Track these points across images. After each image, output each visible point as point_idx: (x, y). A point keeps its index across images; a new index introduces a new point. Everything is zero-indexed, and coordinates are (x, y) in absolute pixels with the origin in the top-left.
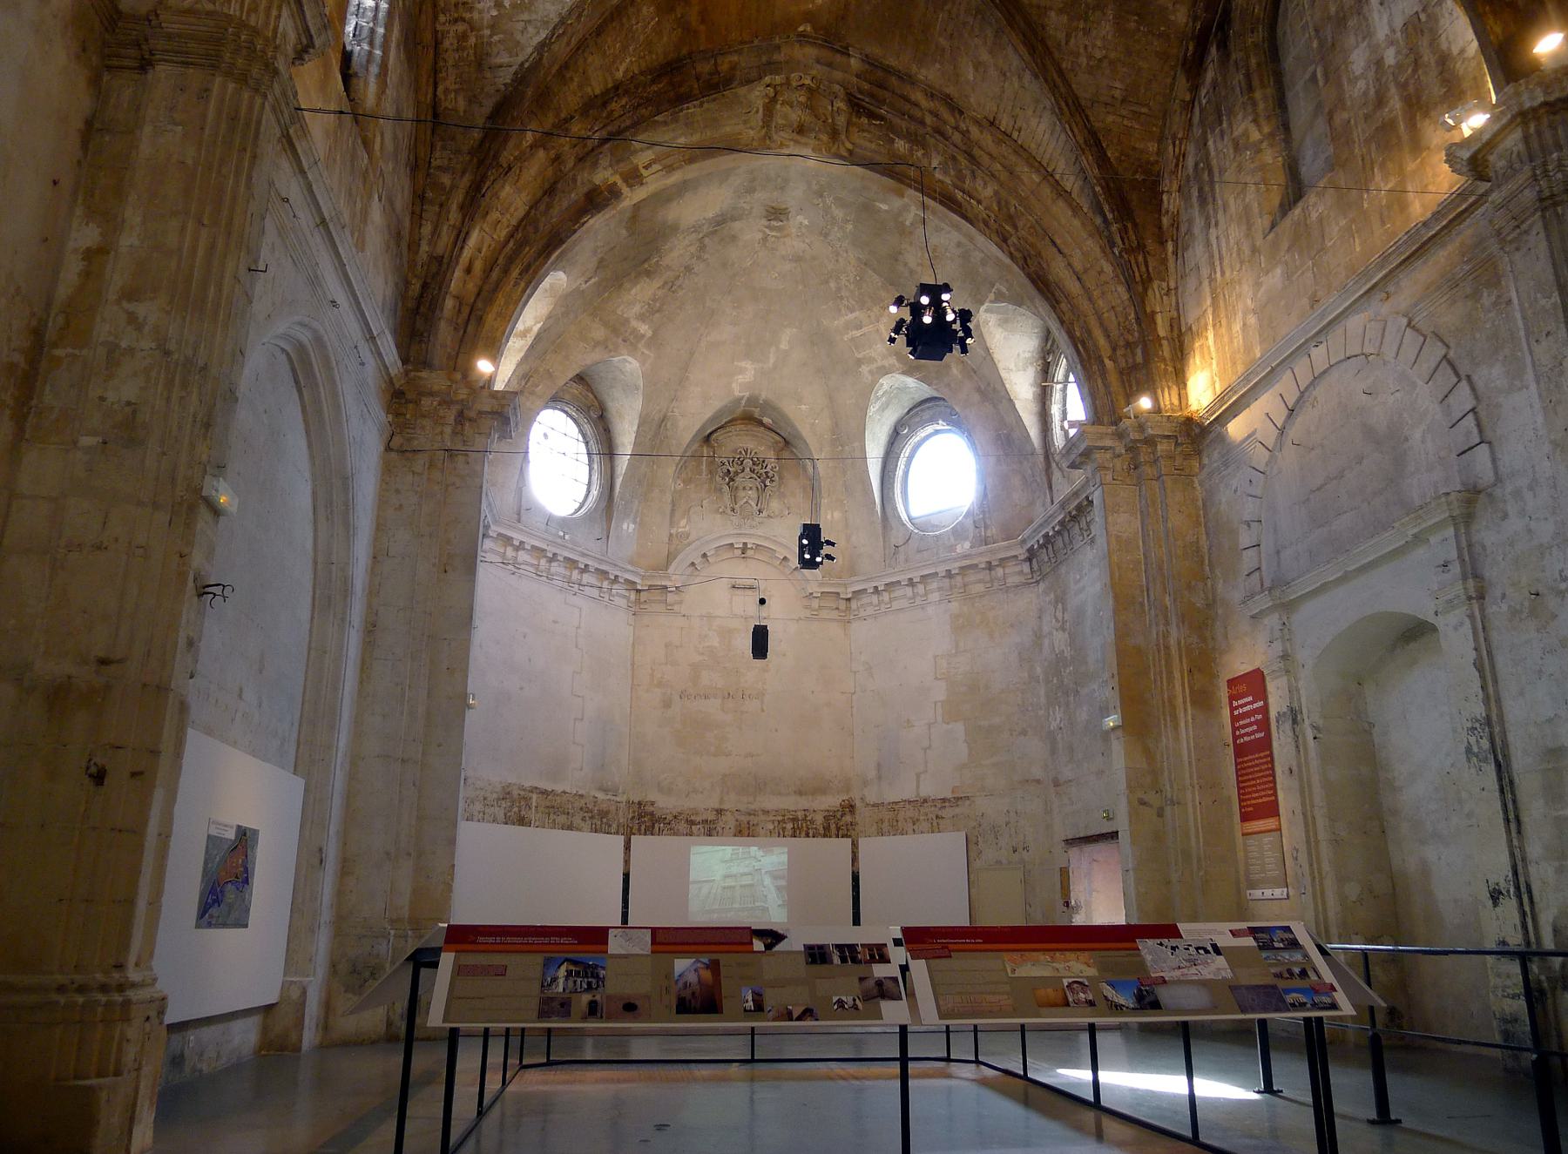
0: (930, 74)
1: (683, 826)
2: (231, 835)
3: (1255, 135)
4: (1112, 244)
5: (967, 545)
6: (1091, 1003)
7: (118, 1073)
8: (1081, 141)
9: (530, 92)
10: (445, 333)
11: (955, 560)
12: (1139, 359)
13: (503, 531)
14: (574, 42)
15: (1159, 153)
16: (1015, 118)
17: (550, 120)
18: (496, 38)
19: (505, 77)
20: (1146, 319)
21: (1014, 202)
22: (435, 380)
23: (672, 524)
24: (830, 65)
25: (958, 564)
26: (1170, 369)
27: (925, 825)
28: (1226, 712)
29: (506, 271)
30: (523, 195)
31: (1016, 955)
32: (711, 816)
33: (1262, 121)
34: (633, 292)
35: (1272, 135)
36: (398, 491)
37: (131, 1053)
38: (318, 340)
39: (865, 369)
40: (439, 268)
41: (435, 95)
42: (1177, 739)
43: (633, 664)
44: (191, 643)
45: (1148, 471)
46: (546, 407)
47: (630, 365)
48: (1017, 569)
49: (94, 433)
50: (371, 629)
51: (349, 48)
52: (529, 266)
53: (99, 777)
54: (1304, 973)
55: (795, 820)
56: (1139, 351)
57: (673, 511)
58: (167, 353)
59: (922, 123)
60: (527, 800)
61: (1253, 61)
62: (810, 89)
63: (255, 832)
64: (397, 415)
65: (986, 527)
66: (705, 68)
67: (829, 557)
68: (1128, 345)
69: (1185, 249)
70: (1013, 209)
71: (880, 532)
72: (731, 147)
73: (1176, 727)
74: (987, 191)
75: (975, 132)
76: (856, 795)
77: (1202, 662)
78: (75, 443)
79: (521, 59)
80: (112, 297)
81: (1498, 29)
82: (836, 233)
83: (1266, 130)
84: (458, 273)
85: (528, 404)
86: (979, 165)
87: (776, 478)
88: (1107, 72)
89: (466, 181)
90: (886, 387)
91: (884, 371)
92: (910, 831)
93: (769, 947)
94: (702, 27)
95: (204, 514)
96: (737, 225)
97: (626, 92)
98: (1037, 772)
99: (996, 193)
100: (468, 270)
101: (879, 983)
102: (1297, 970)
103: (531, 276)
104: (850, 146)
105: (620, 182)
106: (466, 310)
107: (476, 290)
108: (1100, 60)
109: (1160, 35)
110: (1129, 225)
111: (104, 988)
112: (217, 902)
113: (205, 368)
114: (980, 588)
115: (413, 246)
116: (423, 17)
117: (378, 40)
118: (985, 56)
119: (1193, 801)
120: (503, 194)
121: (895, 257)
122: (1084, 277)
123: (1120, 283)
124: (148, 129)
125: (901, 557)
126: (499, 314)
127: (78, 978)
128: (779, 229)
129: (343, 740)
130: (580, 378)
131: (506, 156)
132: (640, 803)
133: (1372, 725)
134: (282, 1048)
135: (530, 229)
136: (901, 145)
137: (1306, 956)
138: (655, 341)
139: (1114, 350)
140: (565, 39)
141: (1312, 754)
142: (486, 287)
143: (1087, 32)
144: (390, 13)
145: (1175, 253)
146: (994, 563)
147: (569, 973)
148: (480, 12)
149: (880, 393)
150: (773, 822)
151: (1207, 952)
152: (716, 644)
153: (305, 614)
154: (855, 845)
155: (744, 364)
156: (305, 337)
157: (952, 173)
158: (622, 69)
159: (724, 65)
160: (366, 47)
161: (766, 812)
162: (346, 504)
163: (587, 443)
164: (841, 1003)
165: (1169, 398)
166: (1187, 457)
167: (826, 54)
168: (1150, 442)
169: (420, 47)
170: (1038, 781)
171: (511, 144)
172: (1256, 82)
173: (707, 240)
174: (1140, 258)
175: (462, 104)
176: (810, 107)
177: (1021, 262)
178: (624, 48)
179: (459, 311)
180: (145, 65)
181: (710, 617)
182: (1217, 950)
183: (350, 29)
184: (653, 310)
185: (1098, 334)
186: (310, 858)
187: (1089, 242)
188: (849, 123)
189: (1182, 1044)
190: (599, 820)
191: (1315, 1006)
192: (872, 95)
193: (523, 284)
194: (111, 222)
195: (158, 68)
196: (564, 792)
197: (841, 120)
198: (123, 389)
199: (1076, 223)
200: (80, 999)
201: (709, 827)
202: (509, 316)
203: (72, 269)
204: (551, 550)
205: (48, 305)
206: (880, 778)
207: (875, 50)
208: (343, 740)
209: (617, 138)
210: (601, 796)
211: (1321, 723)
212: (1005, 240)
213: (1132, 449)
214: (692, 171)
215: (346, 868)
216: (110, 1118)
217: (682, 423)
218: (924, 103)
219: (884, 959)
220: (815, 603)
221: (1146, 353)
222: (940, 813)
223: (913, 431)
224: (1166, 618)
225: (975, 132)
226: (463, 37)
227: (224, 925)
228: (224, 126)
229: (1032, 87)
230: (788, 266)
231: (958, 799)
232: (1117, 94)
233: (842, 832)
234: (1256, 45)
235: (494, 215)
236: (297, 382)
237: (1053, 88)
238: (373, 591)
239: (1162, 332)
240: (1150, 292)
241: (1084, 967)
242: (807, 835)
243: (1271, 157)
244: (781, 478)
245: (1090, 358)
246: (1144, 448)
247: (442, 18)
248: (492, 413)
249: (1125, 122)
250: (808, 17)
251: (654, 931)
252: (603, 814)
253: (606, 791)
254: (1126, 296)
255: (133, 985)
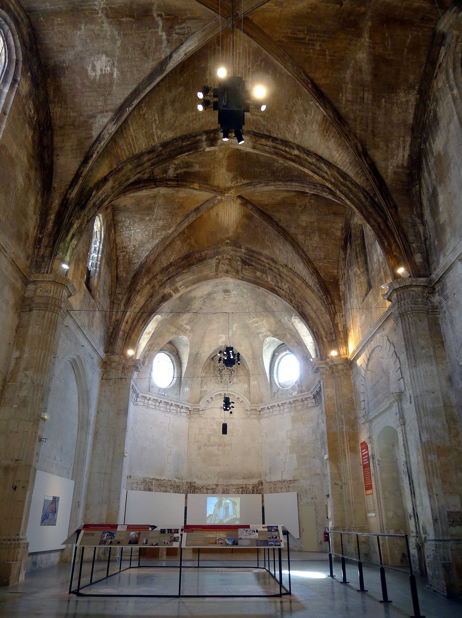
0: (266, 252)
1: (205, 490)
2: (51, 499)
3: (359, 272)
4: (324, 302)
5: (296, 393)
6: (222, 543)
7: (16, 561)
8: (312, 272)
9: (144, 270)
10: (120, 342)
11: (291, 398)
12: (334, 338)
13: (143, 395)
14: (156, 255)
15: (337, 273)
16: (292, 264)
17: (151, 276)
18: (134, 255)
19: (137, 266)
20: (335, 325)
21: (294, 289)
22: (116, 358)
23: (201, 387)
24: (236, 251)
25: (292, 400)
26: (343, 341)
27: (284, 490)
28: (361, 454)
29: (138, 322)
30: (143, 299)
31: (208, 532)
32: (214, 487)
33: (361, 268)
34: (184, 317)
35: (363, 272)
36: (105, 391)
37: (19, 556)
38: (78, 356)
39: (260, 336)
40: (118, 323)
41: (117, 272)
42: (346, 463)
43: (188, 435)
44: (37, 454)
45: (336, 374)
46: (159, 352)
47: (185, 338)
48: (311, 401)
49: (16, 404)
50: (96, 433)
51: (90, 269)
52: (145, 320)
53: (15, 488)
54: (276, 537)
55: (242, 488)
56: (334, 335)
57: (202, 383)
58: (34, 383)
59: (265, 267)
60: (151, 483)
61: (358, 249)
62: (230, 259)
63: (58, 498)
64: (105, 368)
65: (302, 387)
66: (197, 255)
67: (233, 407)
68: (331, 334)
69: (346, 303)
70: (294, 292)
71: (269, 388)
72: (206, 278)
73: (346, 459)
74: (286, 286)
75: (281, 268)
76: (263, 479)
77: (354, 437)
78: (12, 406)
79: (141, 261)
80: (21, 370)
81: (392, 263)
82: (245, 296)
83: (362, 270)
84: (124, 324)
85: (152, 353)
86: (283, 278)
87: (235, 371)
88: (318, 250)
89: (126, 297)
90: (268, 341)
91: (267, 336)
92: (280, 491)
93: (152, 529)
94: (196, 245)
95: (41, 421)
96: (215, 295)
97: (174, 265)
98: (319, 471)
99: (289, 287)
100: (127, 323)
101: (175, 538)
102: (275, 537)
103: (146, 322)
104: (242, 276)
105: (172, 292)
106: (126, 335)
107: (129, 328)
108: (316, 247)
109: (333, 239)
110: (328, 296)
111: (14, 540)
112: (47, 518)
113: (42, 385)
114: (300, 408)
115: (110, 317)
116: (113, 253)
117: (98, 266)
118: (281, 247)
119: (351, 483)
120: (137, 299)
121: (265, 303)
122: (317, 312)
123: (327, 314)
124: (31, 327)
125: (276, 397)
126: (136, 335)
127: (9, 538)
128: (228, 295)
129: (86, 469)
130: (170, 343)
131: (138, 288)
132: (190, 483)
133: (397, 459)
134: (66, 562)
135: (146, 308)
136: (258, 274)
137: (279, 533)
138: (192, 331)
139: (327, 335)
140: (154, 254)
141: (378, 469)
142: (132, 327)
143: (310, 240)
144: (101, 257)
145: (344, 304)
146: (304, 399)
147: (108, 535)
148: (129, 249)
149: (267, 343)
150: (235, 488)
151: (254, 532)
152: (216, 428)
153: (75, 432)
154: (263, 496)
155: (221, 335)
156: (75, 357)
157: (275, 281)
158: (172, 259)
159: (203, 254)
160: (95, 269)
161: (233, 485)
162: (88, 399)
163: (173, 363)
164: (165, 542)
165: (343, 350)
166: (348, 370)
167: (234, 248)
168: (336, 365)
169: (112, 261)
170: (319, 474)
171: (139, 284)
172: (359, 256)
173: (206, 300)
174: (333, 306)
175: (124, 274)
176: (230, 265)
177: (296, 308)
178: (172, 253)
179: (124, 335)
180: (31, 310)
181: (214, 418)
182: (257, 531)
183: (90, 264)
184: (190, 322)
185: (321, 329)
186: (76, 505)
187: (317, 301)
188: (242, 268)
189: (341, 564)
190: (177, 489)
191: (275, 545)
192: (249, 259)
193: (143, 325)
194: (22, 350)
195: (34, 311)
196: (164, 480)
197: (240, 268)
198: (23, 393)
199: (313, 295)
200: (9, 542)
201: (213, 490)
202: (139, 336)
203: (13, 362)
204: (159, 400)
205: (7, 372)
206: (270, 473)
207: (249, 246)
208: (86, 469)
209: (171, 278)
210: (177, 480)
211: (380, 459)
212: (291, 302)
213: (331, 367)
214: (194, 286)
215: (87, 507)
216: (14, 571)
217: (203, 355)
218: (265, 261)
219: (178, 532)
220: (249, 413)
221: (336, 337)
222: (289, 485)
223: (279, 354)
224: (342, 422)
225: (281, 268)
226: (125, 256)
227: (49, 525)
228: (48, 324)
229: (296, 257)
230: (232, 306)
231: (295, 480)
232: (322, 256)
233: (259, 492)
234: (359, 244)
235: (135, 305)
236: (73, 367)
237: (301, 257)
238: (97, 422)
239: (340, 329)
240: (336, 317)
241: (223, 535)
242: (247, 493)
243: (363, 279)
244: (237, 371)
245: (319, 338)
246: (335, 367)
247: (118, 251)
248: (133, 366)
249: (326, 264)
250: (228, 238)
251: (128, 525)
252: (178, 487)
253: (178, 478)
254: (329, 318)
255: (21, 539)
